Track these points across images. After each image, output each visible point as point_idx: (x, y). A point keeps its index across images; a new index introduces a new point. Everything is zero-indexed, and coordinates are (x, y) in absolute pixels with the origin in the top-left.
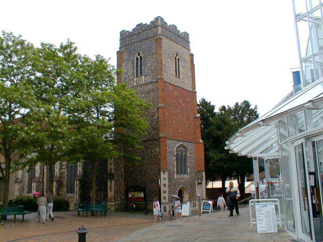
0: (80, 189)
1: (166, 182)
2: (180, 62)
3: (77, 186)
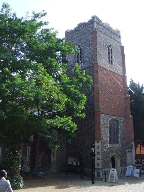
2: (113, 52)
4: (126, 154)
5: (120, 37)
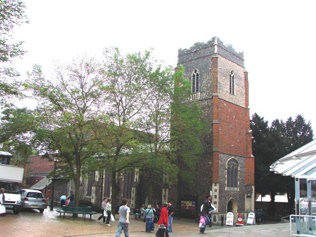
0: (136, 195)
2: (235, 79)
3: (133, 193)
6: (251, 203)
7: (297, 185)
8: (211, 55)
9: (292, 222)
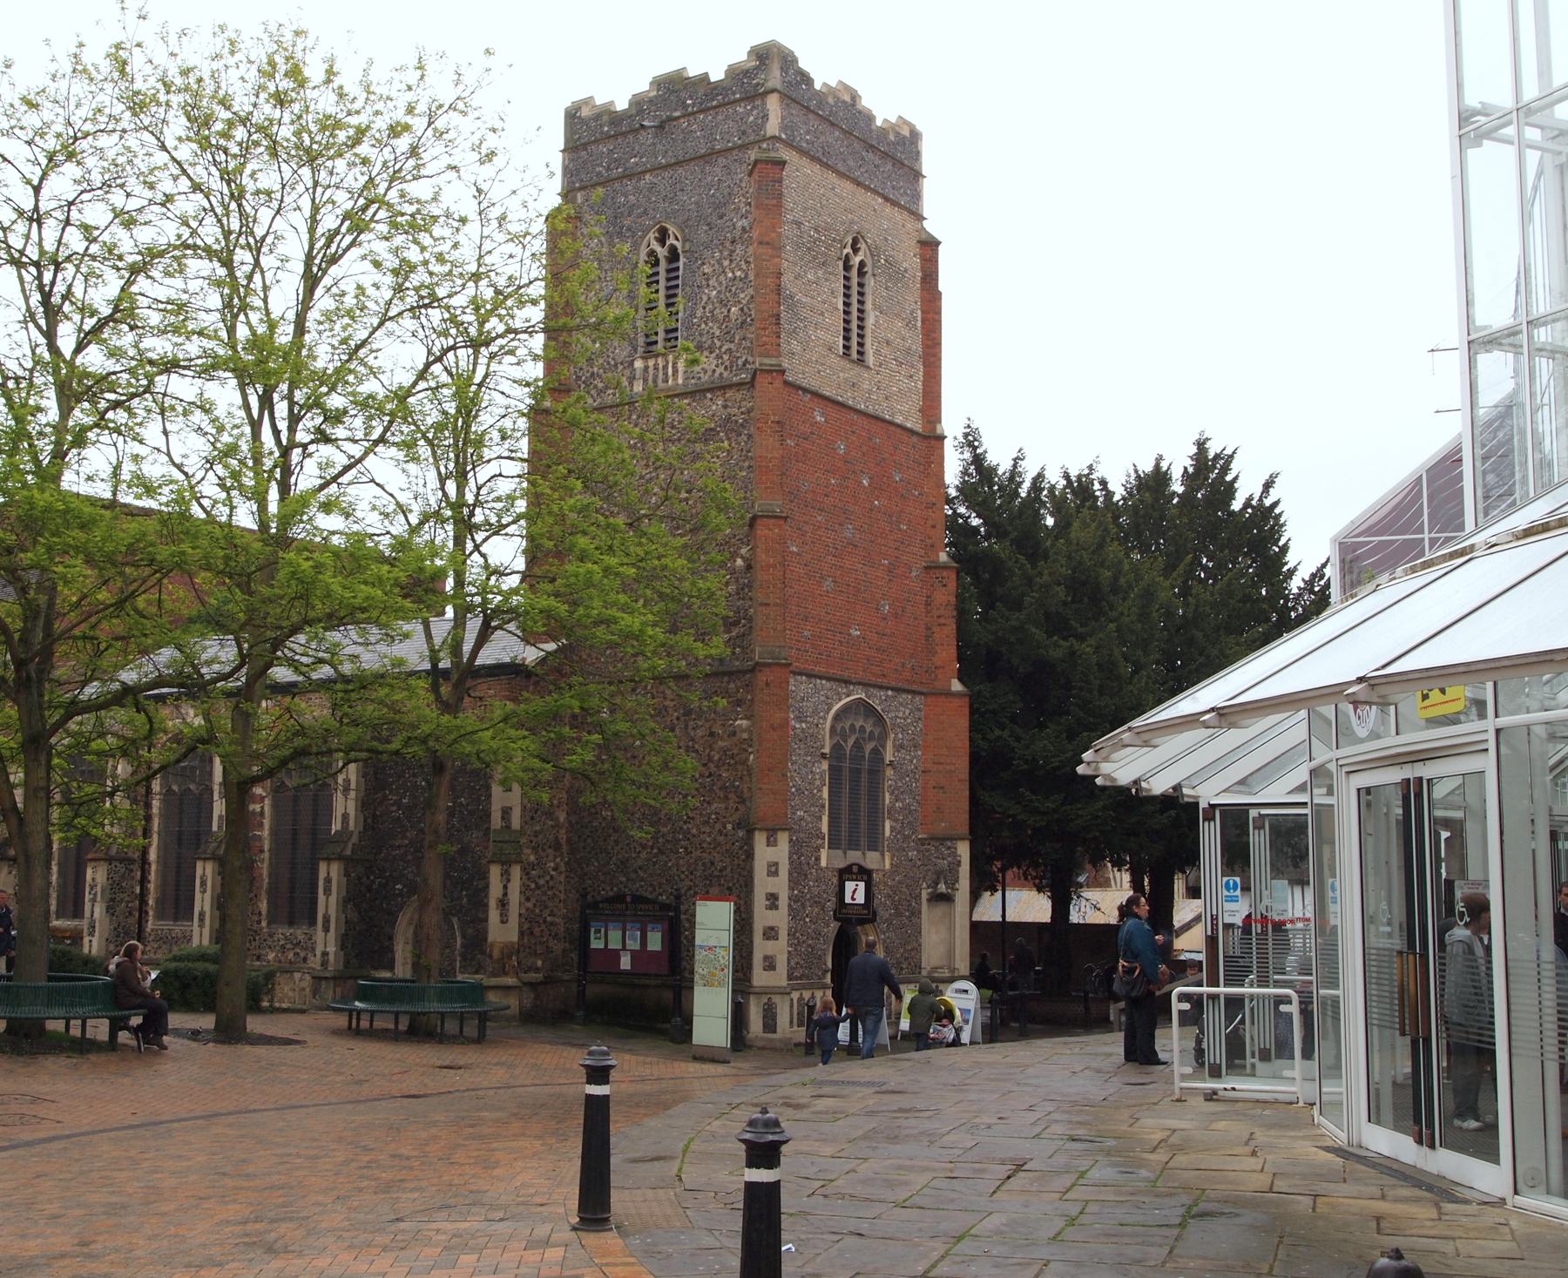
0: (346, 901)
1: (781, 884)
2: (870, 282)
3: (327, 891)
4: (916, 913)
5: (917, 175)
6: (951, 929)
7: (1210, 838)
8: (744, 147)
9: (1182, 1023)
